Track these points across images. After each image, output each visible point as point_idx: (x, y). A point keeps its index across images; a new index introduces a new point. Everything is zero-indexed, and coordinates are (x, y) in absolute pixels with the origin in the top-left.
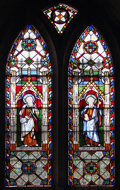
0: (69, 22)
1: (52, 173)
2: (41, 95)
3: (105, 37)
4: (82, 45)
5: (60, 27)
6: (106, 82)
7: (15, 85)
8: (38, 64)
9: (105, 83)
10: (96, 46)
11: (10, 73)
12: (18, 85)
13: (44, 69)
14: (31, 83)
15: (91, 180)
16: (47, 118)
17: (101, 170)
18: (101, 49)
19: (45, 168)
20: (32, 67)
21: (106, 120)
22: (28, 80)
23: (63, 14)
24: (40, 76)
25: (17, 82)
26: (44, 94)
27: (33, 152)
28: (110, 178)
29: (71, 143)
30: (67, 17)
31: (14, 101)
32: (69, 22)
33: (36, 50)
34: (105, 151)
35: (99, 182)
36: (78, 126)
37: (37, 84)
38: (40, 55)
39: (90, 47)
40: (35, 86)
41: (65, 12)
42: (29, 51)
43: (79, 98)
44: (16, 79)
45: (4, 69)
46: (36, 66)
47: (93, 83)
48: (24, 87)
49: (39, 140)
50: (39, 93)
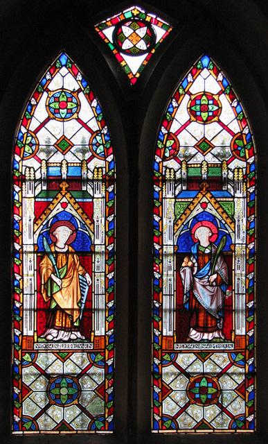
0: (153, 51)
1: (113, 404)
2: (90, 224)
3: (236, 88)
4: (186, 100)
5: (134, 64)
6: (98, 192)
7: (33, 200)
8: (84, 152)
9: (236, 195)
10: (217, 105)
11: (21, 173)
12: (39, 200)
13: (97, 163)
14: (68, 195)
15: (63, 419)
16: (244, 278)
17: (85, 396)
18: (228, 113)
19: (241, 389)
20: (69, 157)
21: (98, 280)
22: (202, 189)
23: (142, 32)
24: (88, 180)
25: (36, 194)
26: (98, 221)
27: (73, 353)
28: (245, 414)
29: (18, 333)
30: (150, 37)
31: (30, 237)
32: (153, 51)
33: (191, 122)
34: (94, 353)
35: (222, 425)
36: (173, 295)
37: (83, 198)
38: (230, 131)
39: (204, 108)
40: (76, 202)
41: (146, 28)
42: (63, 120)
43: (92, 230)
44: (35, 188)
45: (10, 165)
46: (80, 155)
47: (208, 195)
48: (53, 204)
49: (85, 327)
50: (86, 219)
